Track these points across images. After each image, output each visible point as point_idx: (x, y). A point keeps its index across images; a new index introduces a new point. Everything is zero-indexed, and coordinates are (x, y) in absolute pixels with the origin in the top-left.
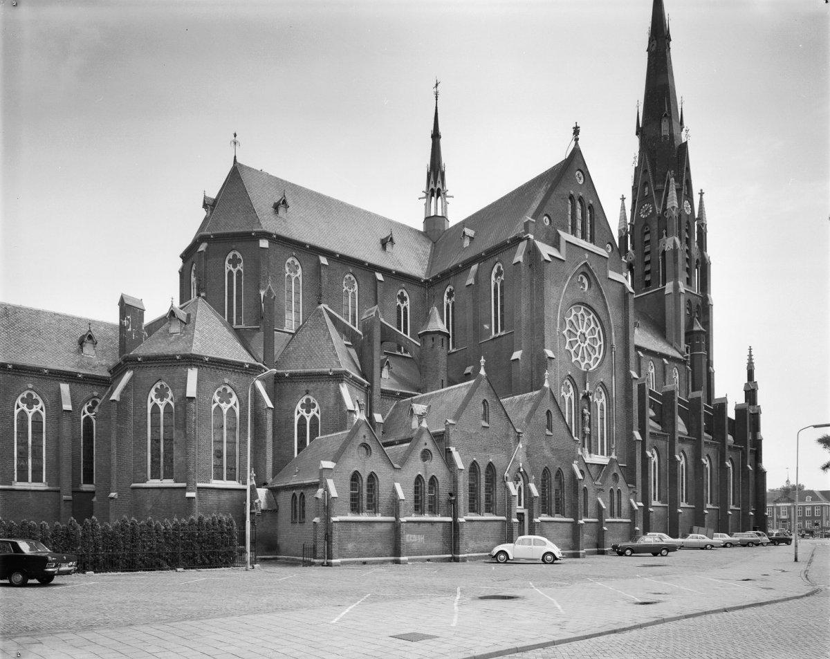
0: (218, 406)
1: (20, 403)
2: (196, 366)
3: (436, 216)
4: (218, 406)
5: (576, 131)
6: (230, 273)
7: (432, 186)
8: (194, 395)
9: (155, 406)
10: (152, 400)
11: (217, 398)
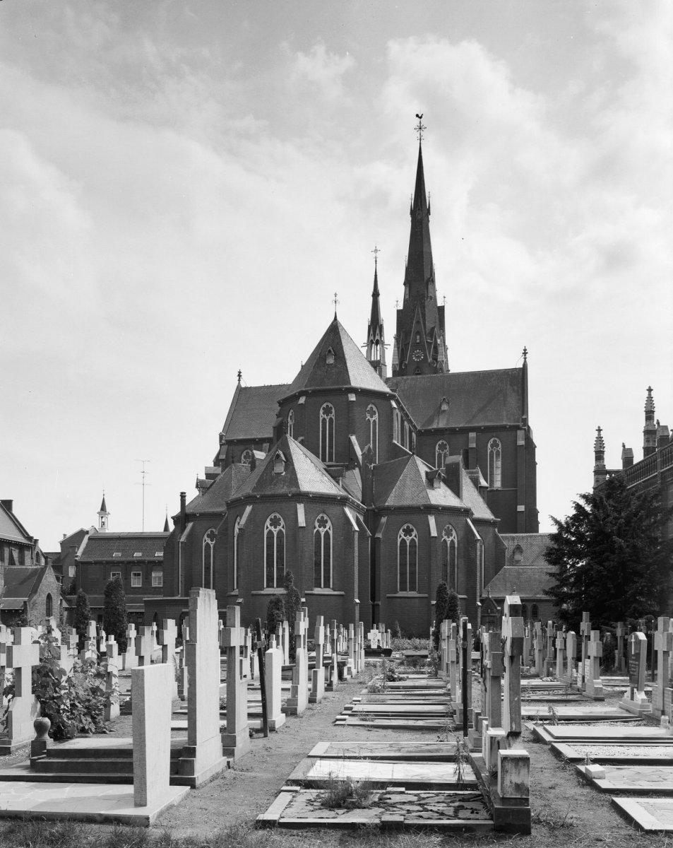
0: (318, 531)
1: (207, 539)
2: (433, 514)
4: (318, 531)
5: (525, 353)
6: (324, 419)
7: (372, 338)
8: (436, 535)
9: (270, 533)
11: (317, 524)
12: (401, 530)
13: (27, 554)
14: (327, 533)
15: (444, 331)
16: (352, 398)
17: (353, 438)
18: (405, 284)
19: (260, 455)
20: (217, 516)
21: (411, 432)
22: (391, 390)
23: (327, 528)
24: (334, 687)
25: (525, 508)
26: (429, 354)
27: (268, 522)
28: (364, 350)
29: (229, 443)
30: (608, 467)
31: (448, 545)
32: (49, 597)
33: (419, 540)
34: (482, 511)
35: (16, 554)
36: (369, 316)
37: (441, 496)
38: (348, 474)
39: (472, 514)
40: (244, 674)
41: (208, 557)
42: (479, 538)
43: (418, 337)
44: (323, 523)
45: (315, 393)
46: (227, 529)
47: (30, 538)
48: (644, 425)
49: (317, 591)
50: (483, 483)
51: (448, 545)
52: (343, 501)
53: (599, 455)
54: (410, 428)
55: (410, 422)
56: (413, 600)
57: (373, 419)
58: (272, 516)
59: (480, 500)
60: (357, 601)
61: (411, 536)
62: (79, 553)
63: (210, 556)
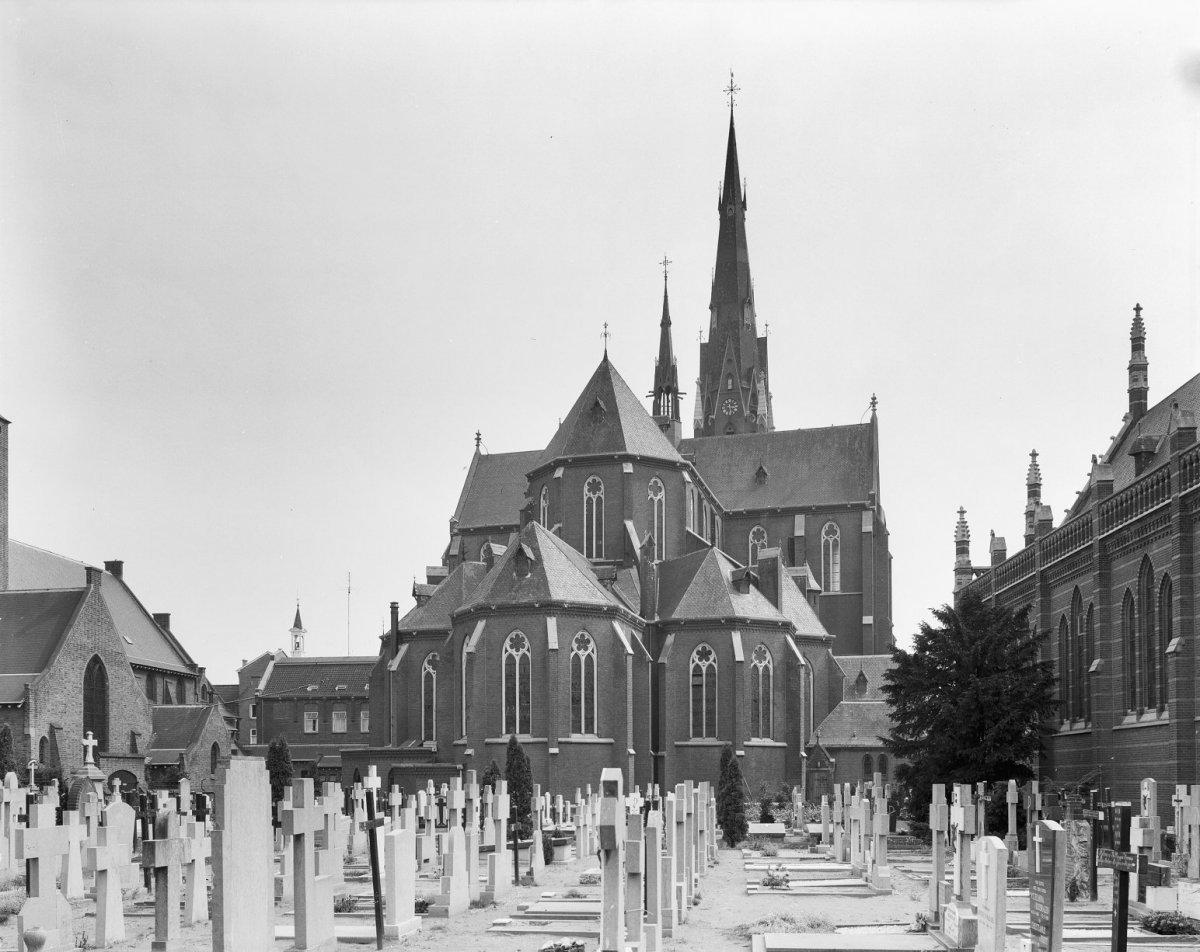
3: (1127, 924)
5: (874, 402)
6: (590, 499)
8: (742, 659)
9: (511, 658)
10: (506, 651)
11: (575, 646)
12: (694, 653)
13: (189, 686)
14: (589, 657)
15: (766, 372)
16: (628, 468)
17: (629, 525)
18: (711, 308)
19: (499, 549)
20: (439, 635)
21: (713, 515)
22: (683, 457)
23: (589, 651)
24: (537, 877)
25: (874, 620)
26: (746, 405)
27: (507, 644)
28: (648, 405)
29: (464, 532)
30: (975, 564)
31: (761, 673)
32: (215, 747)
33: (719, 667)
34: (809, 624)
35: (172, 690)
36: (657, 354)
37: (751, 605)
38: (622, 574)
39: (795, 629)
40: (424, 858)
41: (429, 692)
42: (803, 662)
43: (730, 381)
44: (583, 643)
45: (577, 463)
46: (452, 653)
47: (193, 666)
48: (1026, 503)
49: (575, 738)
50: (813, 584)
51: (761, 673)
52: (612, 613)
53: (962, 548)
54: (711, 509)
55: (712, 501)
56: (712, 750)
57: (659, 497)
58: (513, 635)
59: (808, 609)
60: (632, 751)
61: (708, 660)
62: (262, 685)
63: (432, 690)
